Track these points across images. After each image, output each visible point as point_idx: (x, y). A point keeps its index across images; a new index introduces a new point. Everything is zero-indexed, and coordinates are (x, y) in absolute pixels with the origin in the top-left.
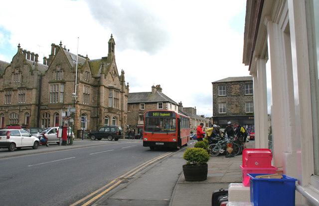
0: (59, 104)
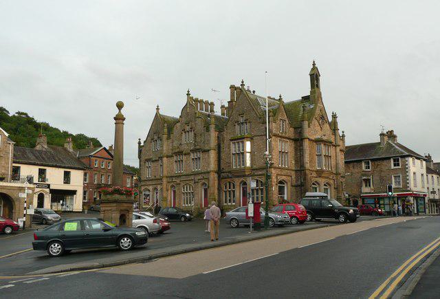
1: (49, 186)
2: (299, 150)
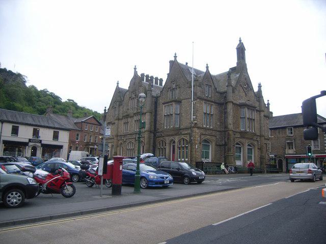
0: (174, 129)
1: (41, 141)
2: (224, 113)
